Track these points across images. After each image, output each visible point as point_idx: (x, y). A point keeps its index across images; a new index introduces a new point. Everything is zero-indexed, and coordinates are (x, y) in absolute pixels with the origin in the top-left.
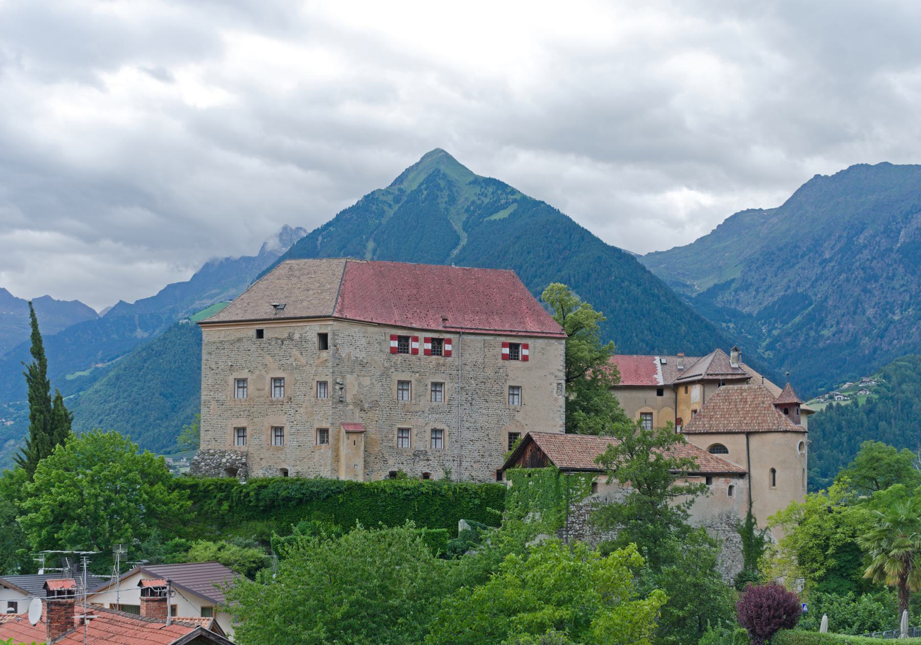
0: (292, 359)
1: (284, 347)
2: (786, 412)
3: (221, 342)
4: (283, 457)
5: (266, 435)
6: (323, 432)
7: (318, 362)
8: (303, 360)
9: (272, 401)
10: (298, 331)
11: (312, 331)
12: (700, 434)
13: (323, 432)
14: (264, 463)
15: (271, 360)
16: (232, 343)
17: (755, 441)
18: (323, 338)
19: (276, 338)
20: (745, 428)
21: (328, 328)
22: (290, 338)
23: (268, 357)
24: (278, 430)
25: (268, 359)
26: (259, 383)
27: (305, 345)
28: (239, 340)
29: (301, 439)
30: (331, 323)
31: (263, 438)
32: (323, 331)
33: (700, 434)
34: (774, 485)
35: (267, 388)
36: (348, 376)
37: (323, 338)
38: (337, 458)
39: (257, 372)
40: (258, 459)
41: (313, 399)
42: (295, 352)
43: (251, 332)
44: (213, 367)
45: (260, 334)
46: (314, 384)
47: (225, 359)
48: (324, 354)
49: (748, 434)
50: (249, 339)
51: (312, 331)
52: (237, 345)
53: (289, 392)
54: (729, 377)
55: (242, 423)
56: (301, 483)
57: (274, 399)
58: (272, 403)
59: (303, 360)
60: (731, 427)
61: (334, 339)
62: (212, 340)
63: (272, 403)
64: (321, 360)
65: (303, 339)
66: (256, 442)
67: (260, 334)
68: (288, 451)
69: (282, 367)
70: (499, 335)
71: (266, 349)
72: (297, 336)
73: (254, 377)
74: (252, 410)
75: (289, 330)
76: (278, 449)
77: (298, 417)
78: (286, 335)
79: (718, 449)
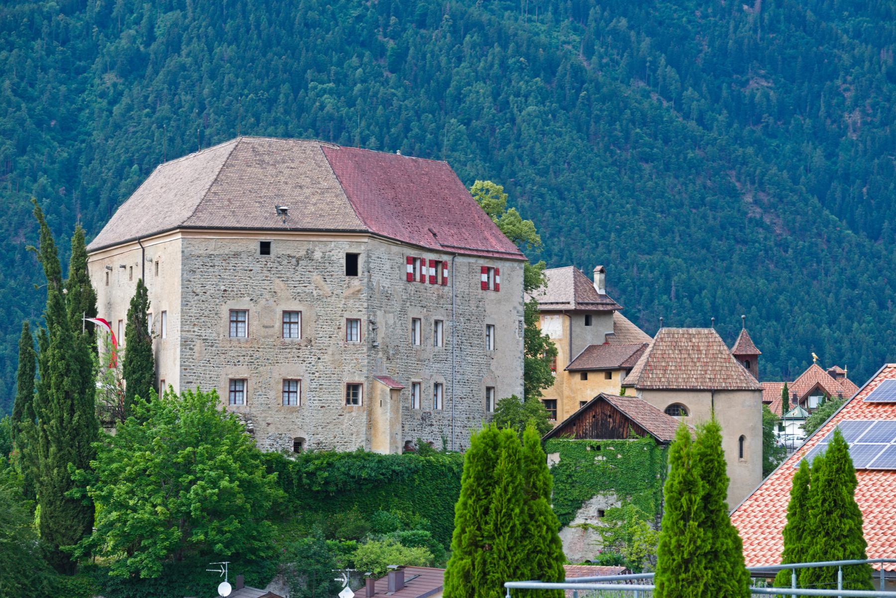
0: (311, 287)
1: (299, 268)
2: (748, 366)
3: (210, 256)
4: (299, 422)
5: (275, 392)
6: (353, 389)
7: (347, 292)
8: (327, 289)
9: (284, 344)
10: (320, 248)
11: (340, 248)
12: (659, 390)
13: (353, 389)
14: (272, 430)
15: (282, 284)
16: (226, 258)
17: (721, 399)
18: (352, 263)
19: (289, 256)
20: (709, 385)
21: (360, 246)
22: (309, 256)
23: (278, 281)
24: (290, 384)
25: (278, 285)
26: (263, 320)
27: (330, 269)
28: (236, 255)
29: (325, 397)
30: (366, 240)
31: (272, 394)
32: (353, 250)
33: (659, 390)
34: (741, 456)
35: (278, 324)
36: (378, 313)
37: (352, 263)
38: (371, 424)
39: (263, 302)
40: (264, 424)
41: (341, 343)
42: (316, 277)
43: (253, 244)
44: (198, 291)
45: (265, 248)
46: (343, 322)
47: (215, 280)
48: (355, 282)
49: (714, 392)
50: (250, 254)
51: (340, 248)
52: (233, 261)
53: (309, 333)
54: (601, 308)
55: (241, 372)
56: (330, 460)
57: (288, 340)
58: (285, 346)
59: (327, 289)
60: (693, 383)
61: (368, 262)
62: (197, 252)
63: (285, 346)
64: (351, 291)
65: (327, 260)
66: (262, 400)
67: (265, 248)
68: (306, 414)
69: (297, 296)
70: (480, 257)
71: (274, 271)
72: (318, 255)
73: (259, 308)
74: (257, 355)
75: (306, 246)
76: (294, 410)
77: (320, 366)
78: (302, 253)
79: (675, 410)
